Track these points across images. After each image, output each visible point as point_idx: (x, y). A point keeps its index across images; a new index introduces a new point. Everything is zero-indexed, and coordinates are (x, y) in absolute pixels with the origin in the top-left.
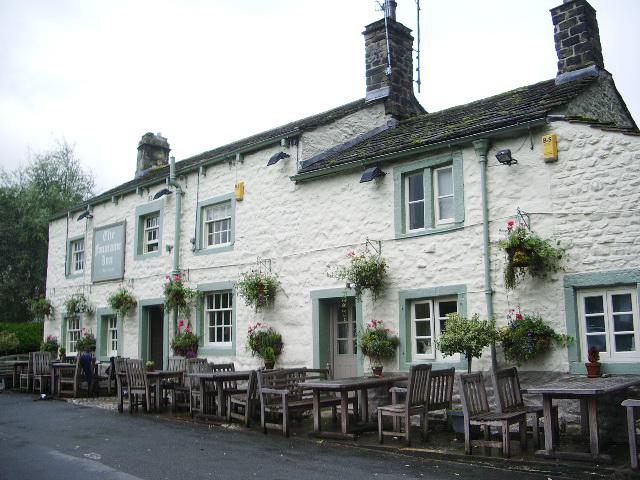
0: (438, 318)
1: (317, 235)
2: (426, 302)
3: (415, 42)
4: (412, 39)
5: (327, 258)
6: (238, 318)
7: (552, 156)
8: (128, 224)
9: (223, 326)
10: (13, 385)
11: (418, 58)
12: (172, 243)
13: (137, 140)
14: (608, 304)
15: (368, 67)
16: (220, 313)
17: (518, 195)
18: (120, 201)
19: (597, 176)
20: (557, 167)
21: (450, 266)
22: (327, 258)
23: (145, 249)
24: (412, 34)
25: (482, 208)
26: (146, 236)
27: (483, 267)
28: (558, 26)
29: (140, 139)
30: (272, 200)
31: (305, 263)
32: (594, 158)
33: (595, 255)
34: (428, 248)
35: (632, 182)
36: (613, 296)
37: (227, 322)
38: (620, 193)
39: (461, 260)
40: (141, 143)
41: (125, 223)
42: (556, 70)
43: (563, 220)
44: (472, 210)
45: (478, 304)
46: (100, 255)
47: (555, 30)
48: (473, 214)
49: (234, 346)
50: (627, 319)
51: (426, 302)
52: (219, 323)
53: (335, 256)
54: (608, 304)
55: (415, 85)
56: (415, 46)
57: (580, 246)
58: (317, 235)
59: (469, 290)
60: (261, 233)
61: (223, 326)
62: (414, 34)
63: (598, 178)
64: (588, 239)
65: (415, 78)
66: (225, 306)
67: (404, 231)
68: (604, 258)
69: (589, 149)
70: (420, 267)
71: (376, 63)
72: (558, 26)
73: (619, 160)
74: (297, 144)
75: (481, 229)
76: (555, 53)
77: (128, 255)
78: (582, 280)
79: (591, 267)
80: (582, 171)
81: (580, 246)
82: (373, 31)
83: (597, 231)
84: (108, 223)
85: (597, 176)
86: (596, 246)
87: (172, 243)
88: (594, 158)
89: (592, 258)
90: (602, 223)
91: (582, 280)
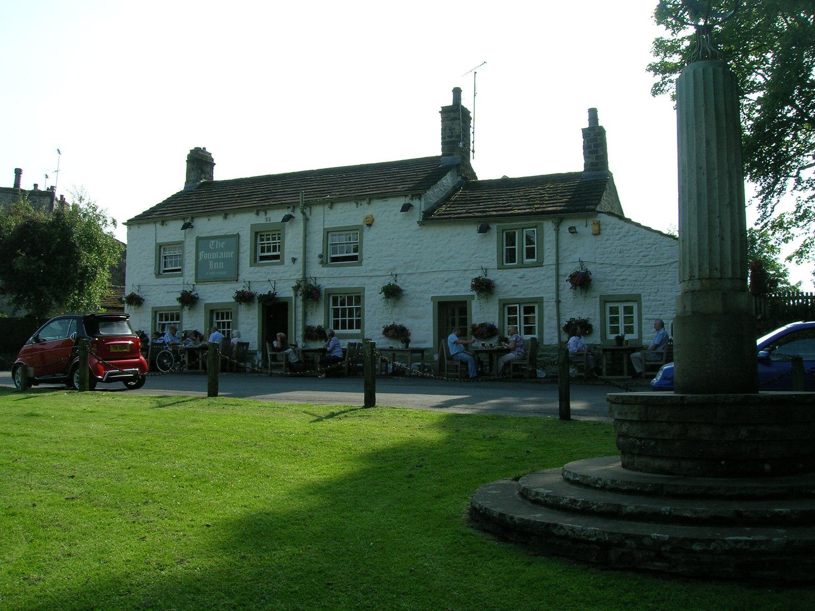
0: (523, 315)
1: (437, 261)
2: (516, 305)
3: (472, 121)
6: (366, 313)
7: (597, 232)
8: (241, 238)
9: (226, 329)
11: (473, 133)
14: (621, 310)
16: (224, 323)
17: (576, 251)
18: (230, 217)
19: (621, 245)
20: (599, 238)
21: (534, 286)
23: (258, 258)
25: (555, 255)
26: (259, 250)
27: (554, 287)
32: (619, 236)
33: (617, 286)
34: (520, 275)
35: (638, 251)
36: (624, 307)
37: (229, 327)
38: (632, 255)
41: (238, 236)
43: (601, 266)
44: (547, 256)
45: (550, 308)
46: (207, 261)
48: (549, 256)
49: (363, 332)
51: (516, 305)
54: (621, 310)
55: (471, 153)
57: (609, 280)
58: (437, 261)
59: (545, 300)
60: (388, 256)
61: (226, 329)
62: (471, 115)
63: (621, 247)
64: (613, 277)
67: (279, 246)
68: (622, 287)
69: (616, 231)
70: (514, 286)
73: (631, 239)
74: (420, 199)
75: (554, 267)
78: (609, 298)
79: (614, 291)
80: (613, 242)
81: (609, 280)
82: (445, 111)
83: (618, 273)
84: (215, 234)
85: (621, 245)
86: (617, 281)
88: (619, 236)
89: (615, 287)
90: (622, 270)
91: (609, 298)
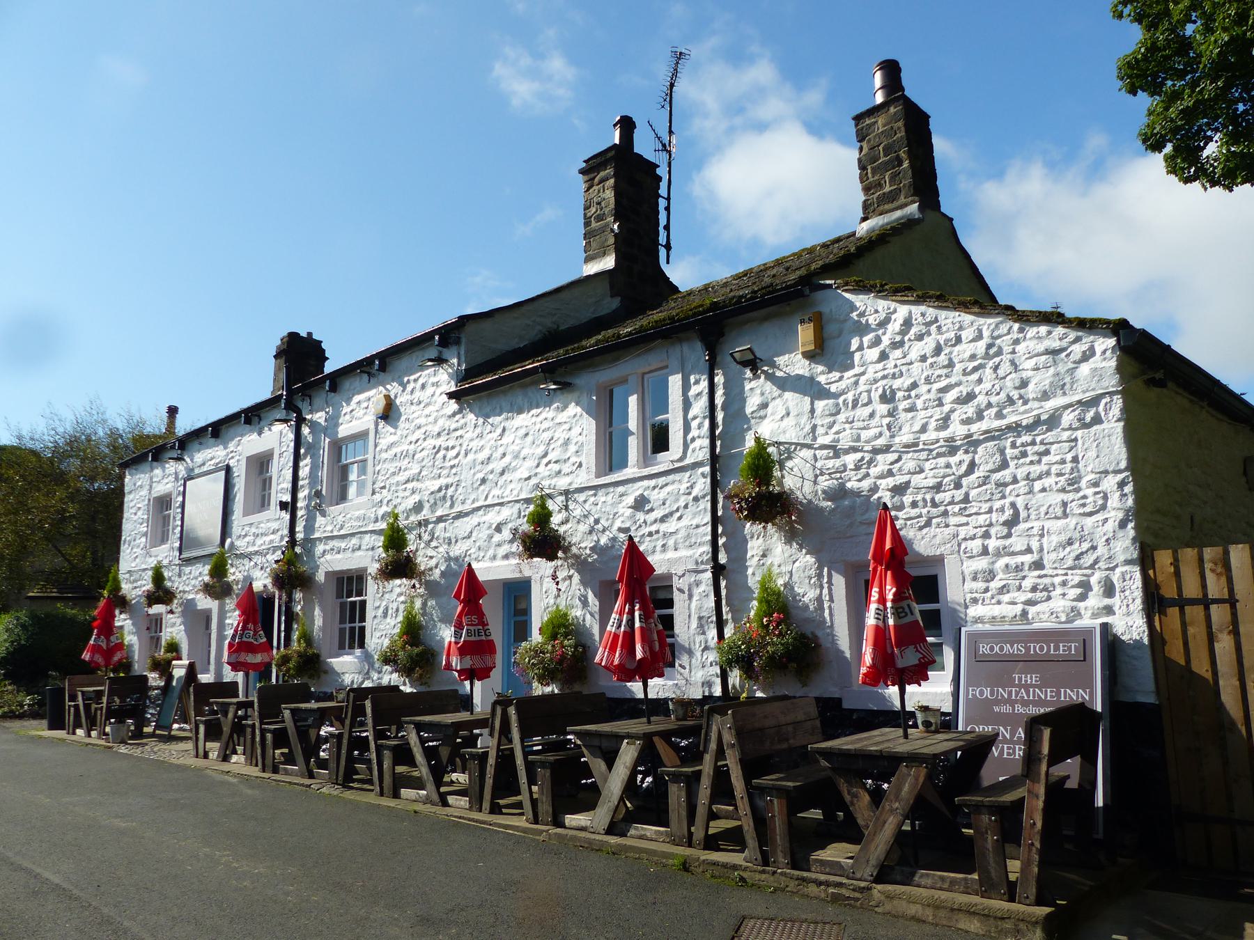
4: (660, 179)
5: (493, 517)
10: (5, 716)
11: (668, 209)
12: (287, 498)
13: (274, 342)
15: (587, 224)
21: (663, 527)
22: (493, 517)
24: (658, 171)
28: (865, 144)
29: (279, 342)
30: (423, 430)
31: (465, 525)
39: (680, 518)
40: (278, 347)
42: (856, 197)
47: (861, 149)
50: (508, 752)
52: (352, 620)
53: (506, 512)
55: (662, 252)
56: (663, 191)
62: (662, 171)
65: (662, 239)
66: (360, 594)
71: (600, 218)
72: (865, 144)
76: (859, 186)
77: (1191, 631)
87: (287, 498)
